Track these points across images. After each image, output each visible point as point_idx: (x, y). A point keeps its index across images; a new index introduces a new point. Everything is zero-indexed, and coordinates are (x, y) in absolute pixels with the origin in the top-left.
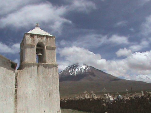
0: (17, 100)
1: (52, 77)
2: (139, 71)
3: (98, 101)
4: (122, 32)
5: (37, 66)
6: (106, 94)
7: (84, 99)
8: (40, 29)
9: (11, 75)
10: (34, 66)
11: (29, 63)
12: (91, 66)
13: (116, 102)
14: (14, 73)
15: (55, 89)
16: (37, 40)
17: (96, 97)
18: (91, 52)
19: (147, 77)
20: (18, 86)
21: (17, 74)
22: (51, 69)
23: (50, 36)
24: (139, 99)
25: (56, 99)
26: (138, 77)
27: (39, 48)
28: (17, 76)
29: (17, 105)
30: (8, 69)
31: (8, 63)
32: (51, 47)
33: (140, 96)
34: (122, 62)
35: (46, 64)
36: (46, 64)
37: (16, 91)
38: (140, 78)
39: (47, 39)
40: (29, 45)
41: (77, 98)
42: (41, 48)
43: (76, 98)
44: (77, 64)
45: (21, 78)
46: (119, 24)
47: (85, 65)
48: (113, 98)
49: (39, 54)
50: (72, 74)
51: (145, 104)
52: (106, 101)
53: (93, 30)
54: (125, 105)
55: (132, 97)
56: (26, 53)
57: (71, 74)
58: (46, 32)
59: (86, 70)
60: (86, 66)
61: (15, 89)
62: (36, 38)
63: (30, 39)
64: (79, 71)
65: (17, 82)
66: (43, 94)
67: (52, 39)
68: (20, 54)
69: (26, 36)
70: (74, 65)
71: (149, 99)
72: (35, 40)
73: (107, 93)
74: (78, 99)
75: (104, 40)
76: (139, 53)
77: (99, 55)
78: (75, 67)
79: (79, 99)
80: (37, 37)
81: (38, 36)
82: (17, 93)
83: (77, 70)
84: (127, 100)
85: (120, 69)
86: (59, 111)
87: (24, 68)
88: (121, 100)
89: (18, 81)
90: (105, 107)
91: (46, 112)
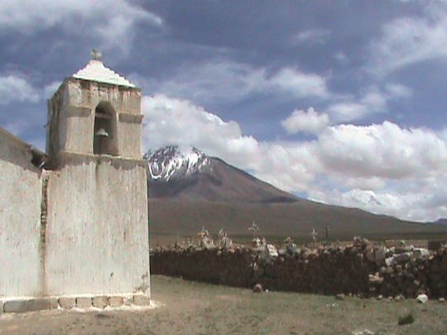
0: (47, 244)
1: (132, 192)
2: (352, 181)
3: (239, 255)
4: (310, 61)
5: (96, 162)
6: (258, 240)
7: (200, 249)
8: (103, 67)
9: (33, 182)
10: (88, 164)
11: (76, 154)
12: (215, 156)
13: (283, 259)
14: (39, 177)
15: (138, 220)
16: (97, 96)
17: (231, 245)
18: (211, 115)
19: (372, 197)
20: (48, 211)
21: (47, 181)
22: (130, 172)
23: (130, 88)
24: (341, 254)
25: (140, 247)
26: (345, 195)
27: (100, 116)
28: (46, 187)
29: (45, 257)
30: (25, 169)
31: (23, 153)
32: (131, 116)
33: (342, 248)
34: (303, 150)
35: (119, 157)
36: (119, 157)
37: (43, 224)
38: (353, 199)
39: (122, 94)
40: (78, 108)
41: (182, 246)
42: (105, 116)
43: (179, 247)
44: (173, 148)
45: (57, 191)
46: (303, 36)
47: (195, 150)
48: (278, 252)
49: (99, 133)
50: (156, 177)
51: (353, 267)
52: (259, 257)
53: (224, 50)
54: (305, 269)
55: (324, 250)
56: (68, 129)
57: (154, 175)
58: (118, 75)
59: (200, 167)
60: (200, 156)
61: (42, 218)
62: (95, 90)
63: (79, 93)
64: (179, 168)
65: (45, 201)
66: (108, 232)
67: (133, 94)
68: (48, 128)
69: (69, 85)
70: (163, 151)
71: (362, 255)
72: (92, 95)
73: (261, 238)
74: (184, 250)
75: (255, 80)
76: (352, 127)
77: (235, 127)
78: (166, 154)
79: (186, 249)
80: (97, 88)
81: (99, 87)
82: (47, 229)
83: (173, 166)
84: (311, 257)
85: (296, 168)
86: (146, 276)
87: (64, 167)
88: (297, 256)
89: (48, 199)
90: (257, 272)
91: (113, 276)
